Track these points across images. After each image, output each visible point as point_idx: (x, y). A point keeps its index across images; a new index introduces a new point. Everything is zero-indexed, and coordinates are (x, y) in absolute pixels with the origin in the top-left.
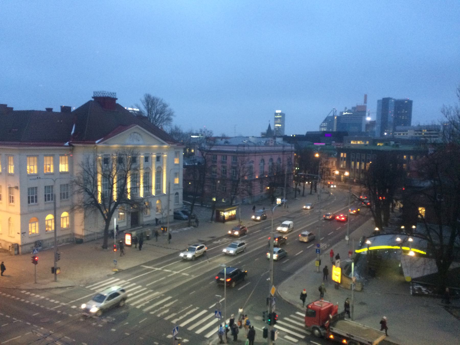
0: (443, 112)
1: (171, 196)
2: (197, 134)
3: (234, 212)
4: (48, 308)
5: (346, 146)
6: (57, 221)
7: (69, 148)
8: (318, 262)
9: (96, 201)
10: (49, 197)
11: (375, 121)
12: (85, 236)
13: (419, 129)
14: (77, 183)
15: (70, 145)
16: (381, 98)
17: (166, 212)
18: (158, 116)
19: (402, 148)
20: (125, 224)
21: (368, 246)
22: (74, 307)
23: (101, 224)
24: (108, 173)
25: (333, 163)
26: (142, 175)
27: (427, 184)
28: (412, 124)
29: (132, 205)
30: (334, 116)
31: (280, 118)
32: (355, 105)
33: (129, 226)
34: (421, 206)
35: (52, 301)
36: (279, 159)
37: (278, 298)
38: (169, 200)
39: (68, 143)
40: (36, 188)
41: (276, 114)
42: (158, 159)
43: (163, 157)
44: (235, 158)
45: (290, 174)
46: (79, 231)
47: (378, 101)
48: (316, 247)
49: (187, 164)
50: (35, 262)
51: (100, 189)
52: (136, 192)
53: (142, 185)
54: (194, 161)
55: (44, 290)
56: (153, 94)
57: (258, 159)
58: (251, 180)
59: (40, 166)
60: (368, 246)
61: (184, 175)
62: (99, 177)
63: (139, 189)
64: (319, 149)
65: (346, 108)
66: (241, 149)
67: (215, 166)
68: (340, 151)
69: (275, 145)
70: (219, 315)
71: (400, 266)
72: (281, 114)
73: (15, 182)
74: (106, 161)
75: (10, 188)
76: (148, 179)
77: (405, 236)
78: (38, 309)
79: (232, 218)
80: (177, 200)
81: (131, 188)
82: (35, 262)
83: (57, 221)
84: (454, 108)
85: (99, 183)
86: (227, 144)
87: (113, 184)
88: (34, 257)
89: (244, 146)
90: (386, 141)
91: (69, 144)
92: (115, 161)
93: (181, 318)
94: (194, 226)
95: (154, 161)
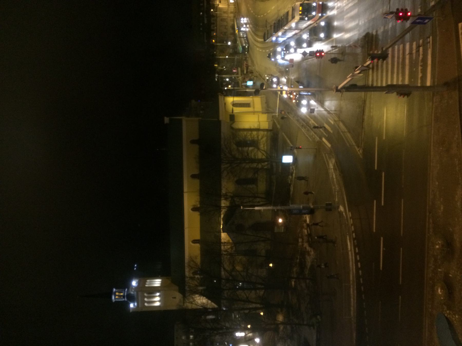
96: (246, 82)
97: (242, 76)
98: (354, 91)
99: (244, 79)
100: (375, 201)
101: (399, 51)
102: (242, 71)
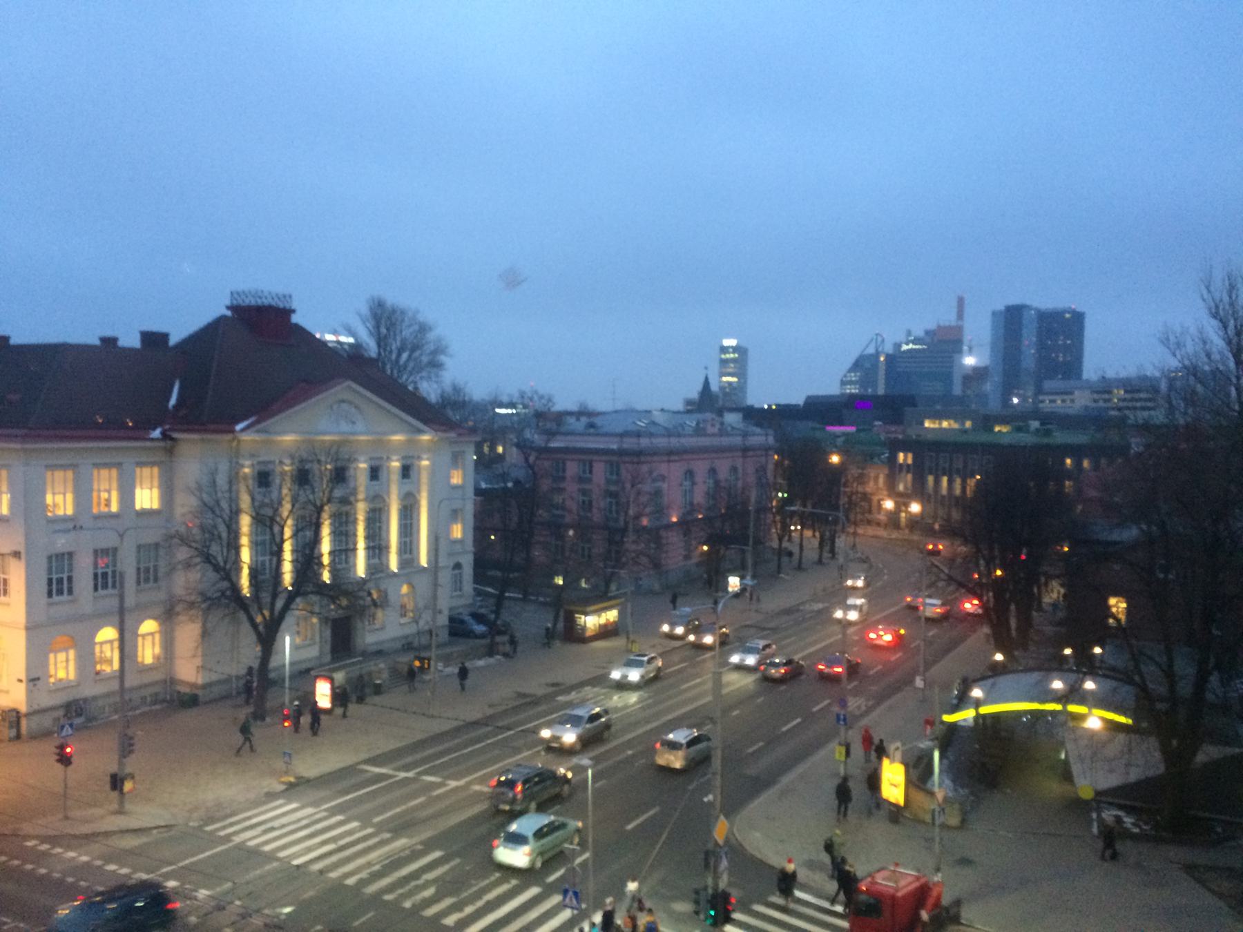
0: (1165, 341)
1: (440, 574)
2: (511, 405)
3: (612, 615)
5: (912, 433)
6: (126, 644)
7: (162, 444)
8: (843, 750)
9: (236, 589)
10: (102, 580)
11: (986, 369)
13: (1104, 387)
14: (185, 540)
15: (165, 436)
16: (1000, 307)
18: (405, 356)
19: (1060, 437)
20: (313, 652)
21: (978, 703)
23: (250, 652)
25: (876, 480)
26: (361, 517)
27: (1130, 533)
28: (1085, 376)
29: (333, 599)
30: (877, 354)
31: (734, 361)
32: (932, 326)
33: (328, 658)
34: (1115, 595)
36: (734, 469)
37: (735, 850)
38: (436, 585)
40: (71, 554)
41: (724, 350)
42: (406, 471)
43: (419, 467)
44: (614, 468)
45: (762, 509)
46: (189, 672)
47: (994, 314)
48: (836, 709)
49: (483, 485)
50: (65, 760)
51: (246, 555)
52: (347, 562)
54: (504, 477)
56: (393, 298)
57: (675, 471)
58: (658, 529)
59: (83, 495)
60: (978, 703)
62: (245, 522)
63: (355, 556)
64: (840, 441)
65: (909, 333)
66: (629, 443)
67: (561, 490)
68: (896, 446)
69: (723, 432)
70: (574, 901)
71: (1063, 756)
72: (735, 349)
74: (264, 478)
77: (1073, 676)
79: (606, 632)
80: (457, 583)
81: (331, 553)
82: (65, 760)
83: (126, 644)
84: (1193, 330)
85: (244, 540)
86: (592, 430)
88: (62, 748)
89: (638, 435)
90: (1017, 419)
91: (163, 433)
92: (288, 479)
93: (469, 910)
94: (506, 655)
95: (395, 477)
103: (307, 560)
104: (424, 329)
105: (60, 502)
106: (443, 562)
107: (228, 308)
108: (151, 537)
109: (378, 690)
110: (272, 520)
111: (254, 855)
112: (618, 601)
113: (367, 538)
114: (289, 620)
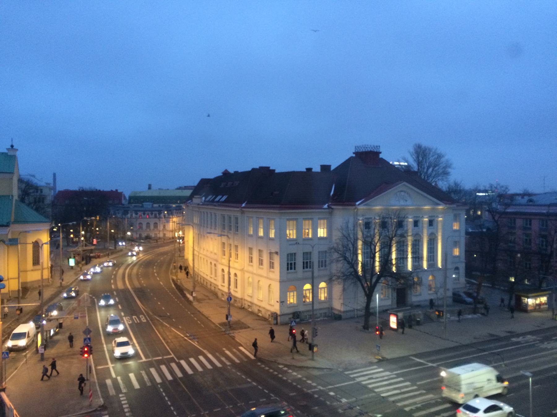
4: (305, 390)
6: (315, 291)
7: (327, 210)
9: (356, 272)
10: (307, 265)
12: (344, 312)
14: (336, 250)
15: (329, 207)
17: (441, 291)
18: (431, 170)
22: (332, 394)
23: (362, 300)
24: (369, 240)
26: (410, 243)
35: (309, 382)
39: (327, 205)
40: (295, 254)
42: (431, 223)
46: (338, 305)
49: (470, 230)
51: (360, 258)
53: (410, 256)
54: (481, 226)
55: (301, 368)
56: (425, 143)
59: (299, 231)
61: (466, 245)
62: (360, 243)
63: (407, 261)
73: (275, 248)
74: (367, 225)
75: (271, 253)
76: (418, 249)
78: (295, 389)
81: (396, 259)
83: (315, 291)
85: (360, 251)
86: (531, 203)
87: (375, 253)
88: (291, 330)
91: (328, 206)
92: (377, 225)
94: (482, 314)
95: (426, 225)
96: (74, 257)
97: (81, 251)
98: (173, 370)
99: (79, 255)
100: (215, 410)
101: (388, 391)
102: (91, 251)
103: (386, 261)
104: (440, 156)
105: (291, 234)
106: (449, 266)
107: (354, 153)
108: (324, 248)
109: (418, 323)
110: (371, 243)
111: (364, 388)
112: (547, 292)
113: (413, 253)
114: (379, 287)
